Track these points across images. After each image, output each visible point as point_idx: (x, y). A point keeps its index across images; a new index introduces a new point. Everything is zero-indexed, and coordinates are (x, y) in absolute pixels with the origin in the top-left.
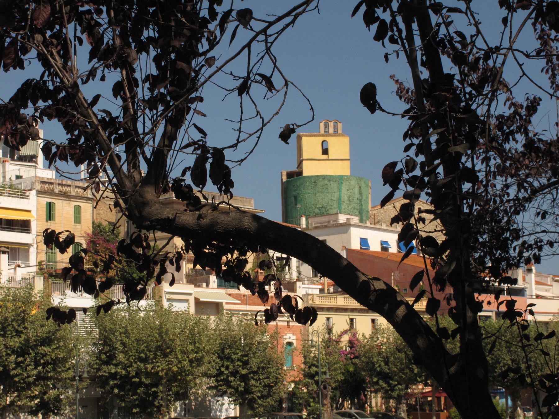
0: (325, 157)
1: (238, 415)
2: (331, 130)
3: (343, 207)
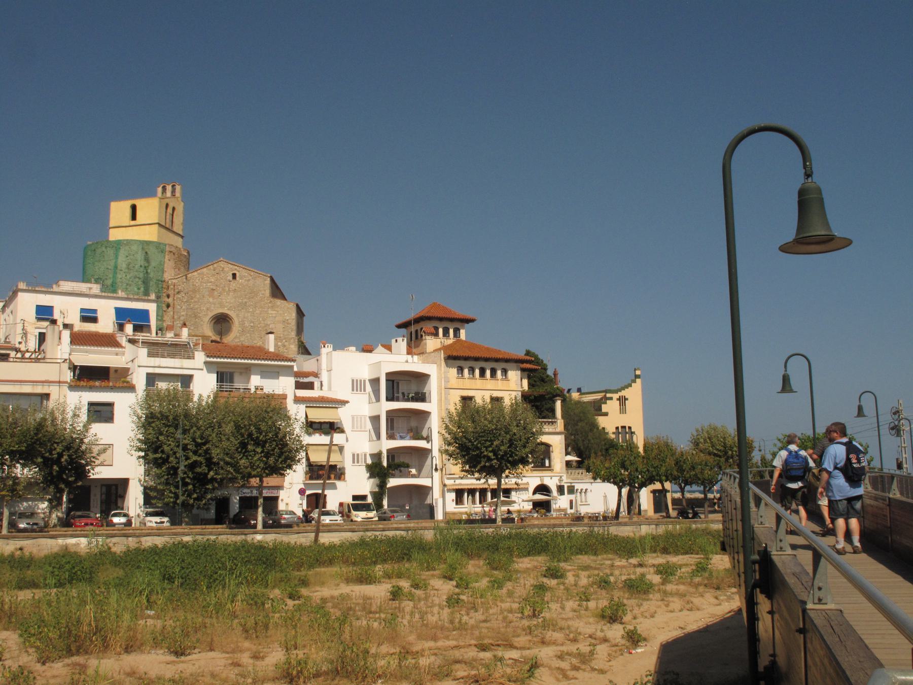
0: (133, 223)
2: (169, 194)
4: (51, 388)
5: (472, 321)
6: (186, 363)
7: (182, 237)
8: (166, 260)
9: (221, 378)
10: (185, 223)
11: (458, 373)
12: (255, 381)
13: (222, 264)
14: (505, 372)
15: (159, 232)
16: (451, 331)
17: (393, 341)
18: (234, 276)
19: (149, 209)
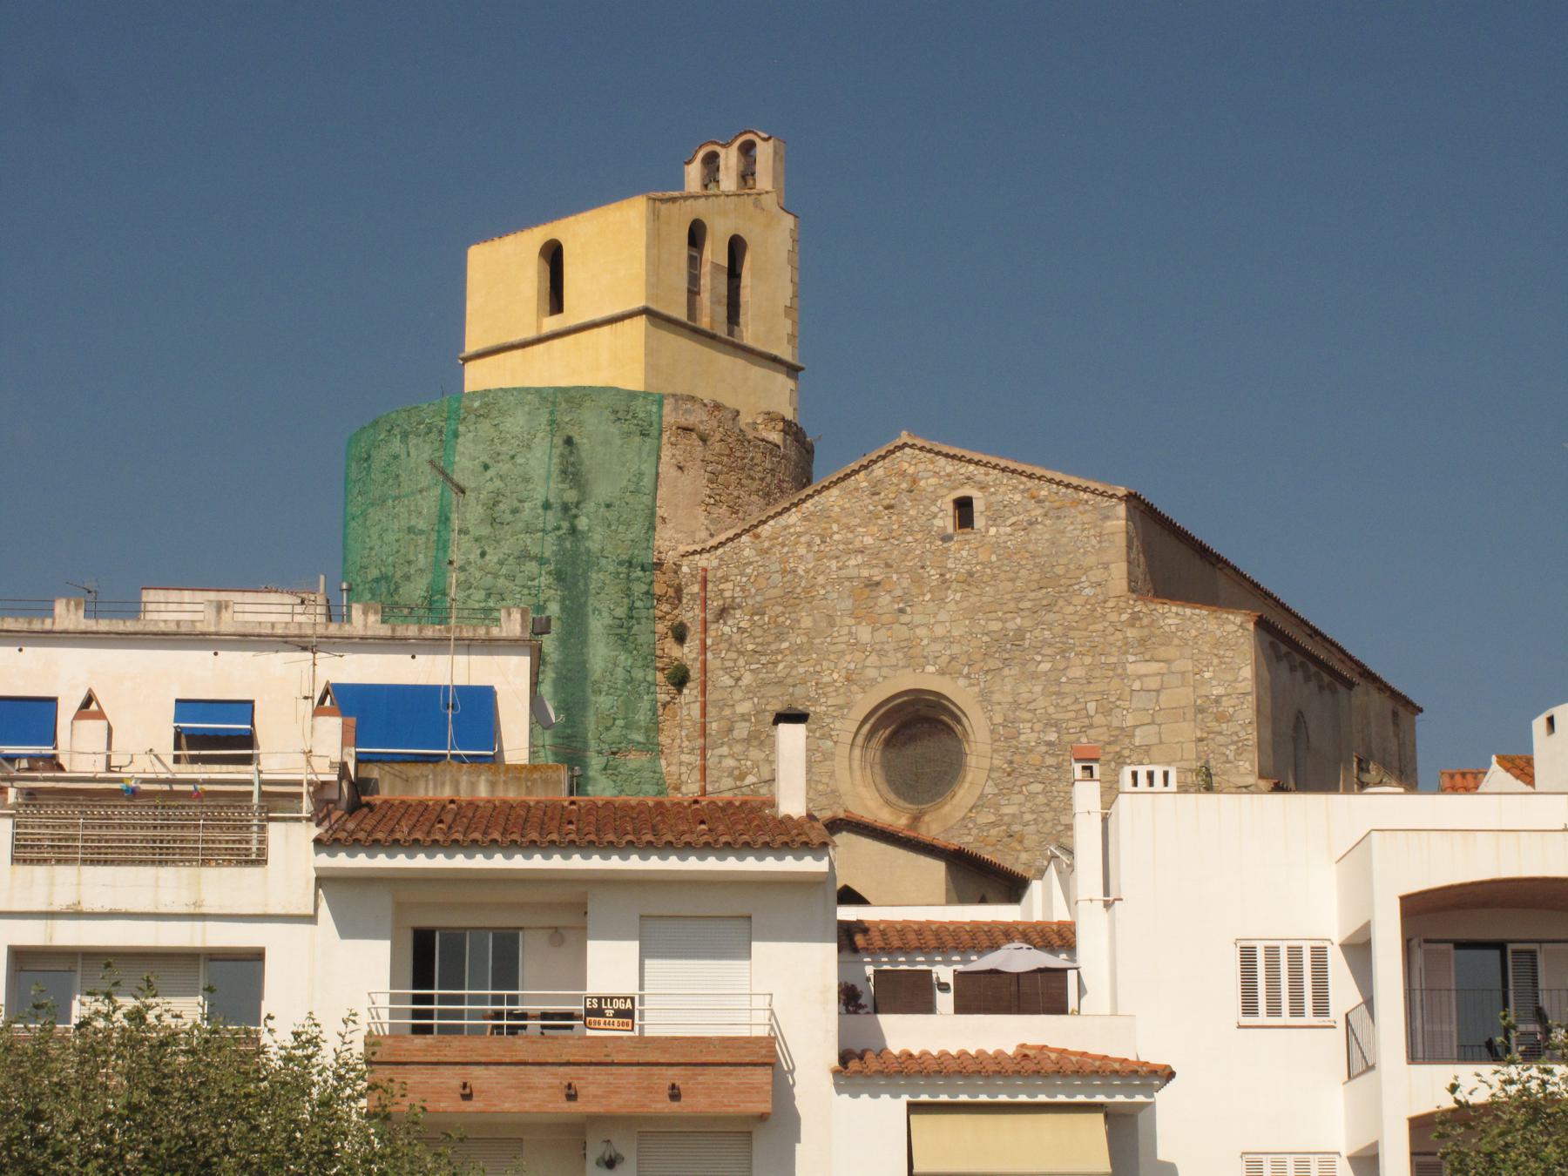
0: (552, 323)
6: (222, 886)
7: (793, 370)
9: (426, 960)
10: (804, 306)
12: (610, 965)
13: (906, 461)
17: (1539, 724)
18: (964, 507)
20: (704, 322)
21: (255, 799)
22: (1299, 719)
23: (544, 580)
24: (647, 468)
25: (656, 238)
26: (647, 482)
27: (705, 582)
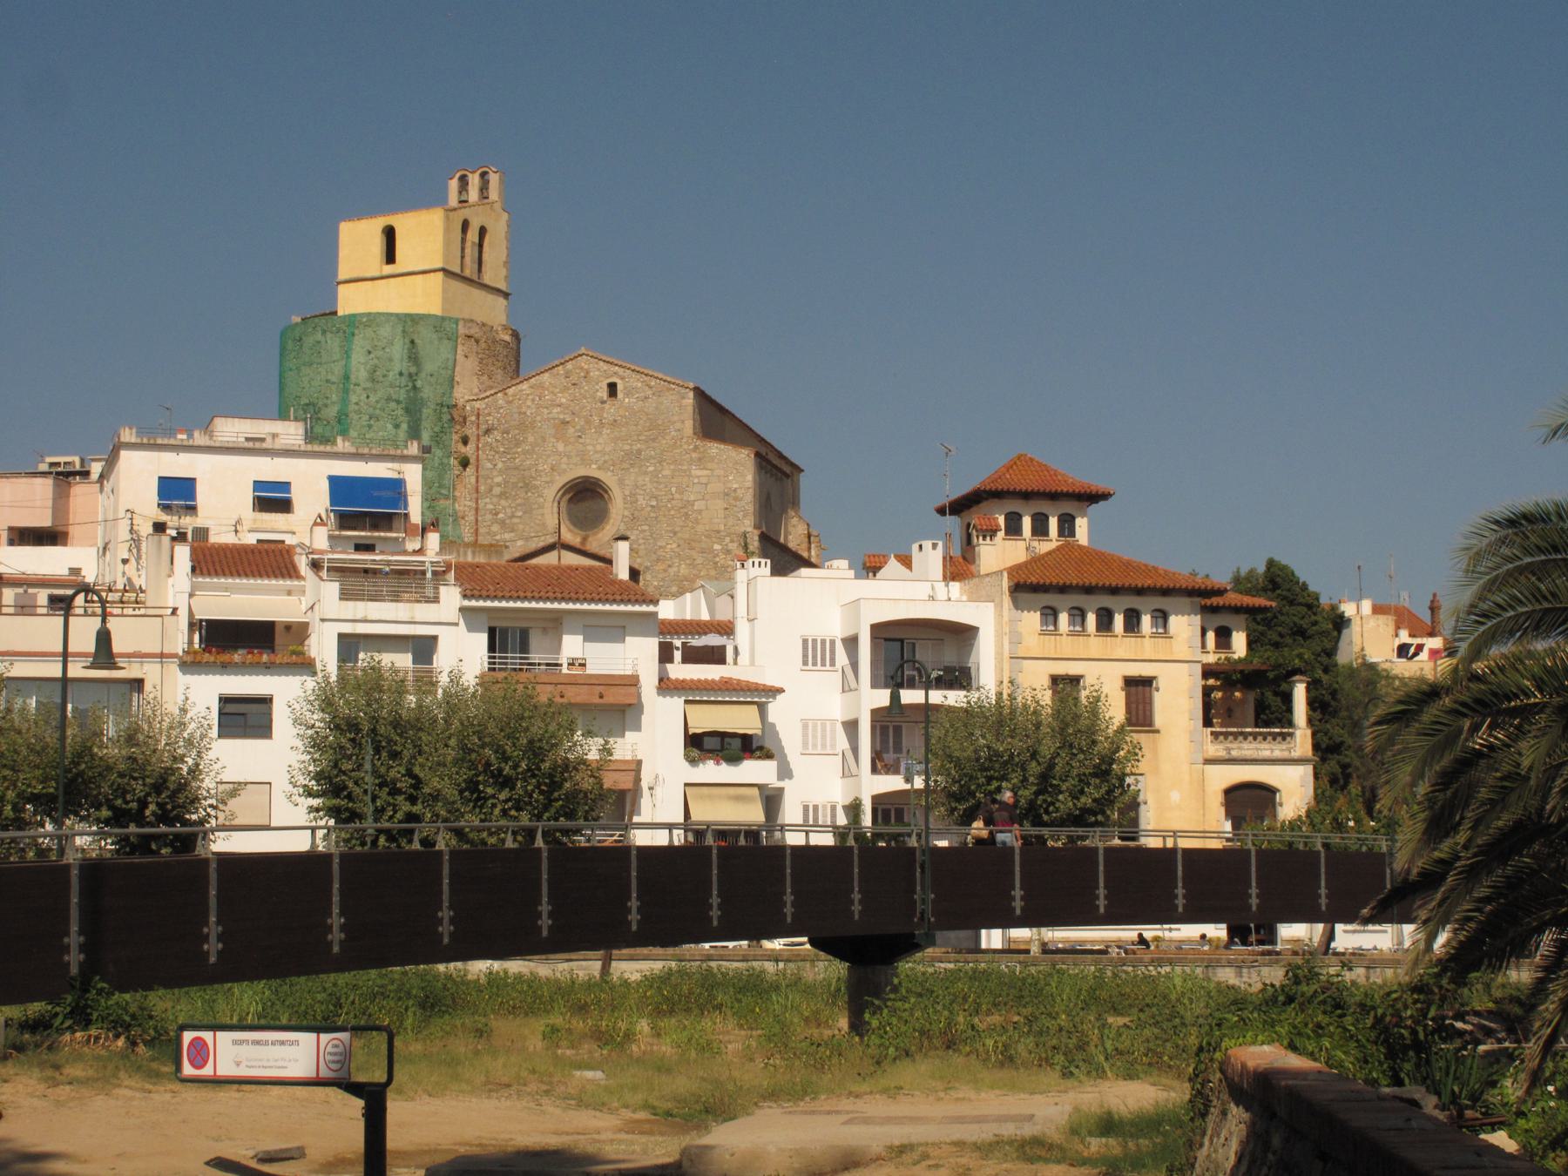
0: (388, 269)
1: (983, 932)
2: (473, 195)
3: (354, 399)
4: (146, 667)
5: (1105, 496)
6: (423, 611)
7: (506, 295)
8: (460, 357)
9: (497, 640)
11: (1044, 622)
12: (572, 646)
14: (1162, 617)
15: (445, 291)
16: (1053, 523)
17: (915, 547)
18: (612, 388)
19: (424, 236)
20: (467, 273)
21: (429, 575)
22: (768, 498)
23: (400, 412)
24: (451, 356)
25: (447, 230)
26: (450, 363)
27: (478, 416)
